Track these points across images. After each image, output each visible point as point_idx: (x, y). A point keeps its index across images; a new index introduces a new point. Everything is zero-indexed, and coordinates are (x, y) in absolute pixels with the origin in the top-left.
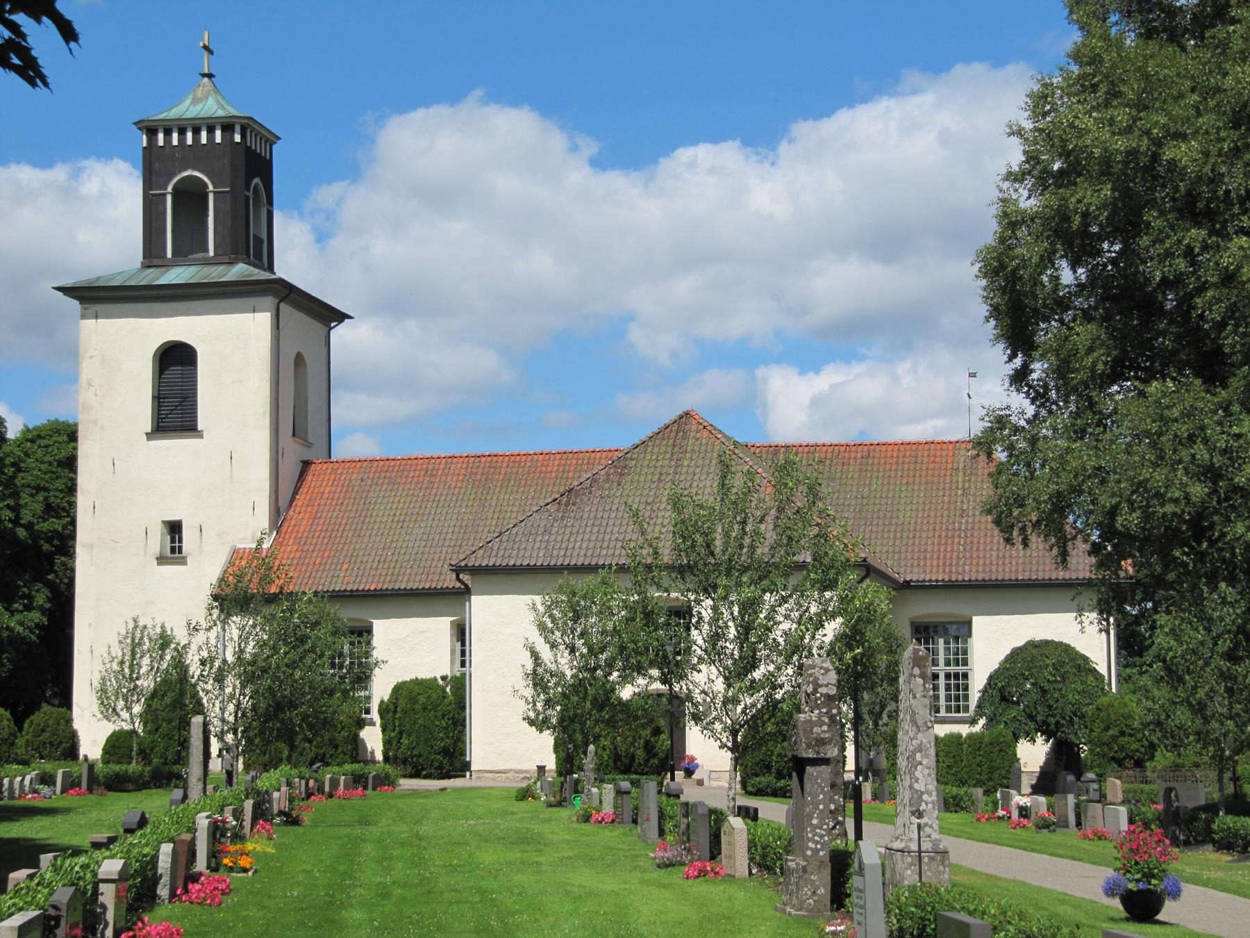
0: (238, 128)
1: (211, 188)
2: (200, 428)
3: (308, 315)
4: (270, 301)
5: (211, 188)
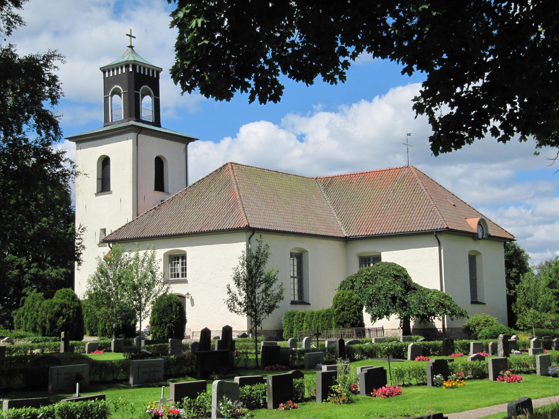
0: (131, 66)
1: (122, 91)
2: (111, 189)
3: (176, 141)
4: (133, 135)
5: (122, 91)
